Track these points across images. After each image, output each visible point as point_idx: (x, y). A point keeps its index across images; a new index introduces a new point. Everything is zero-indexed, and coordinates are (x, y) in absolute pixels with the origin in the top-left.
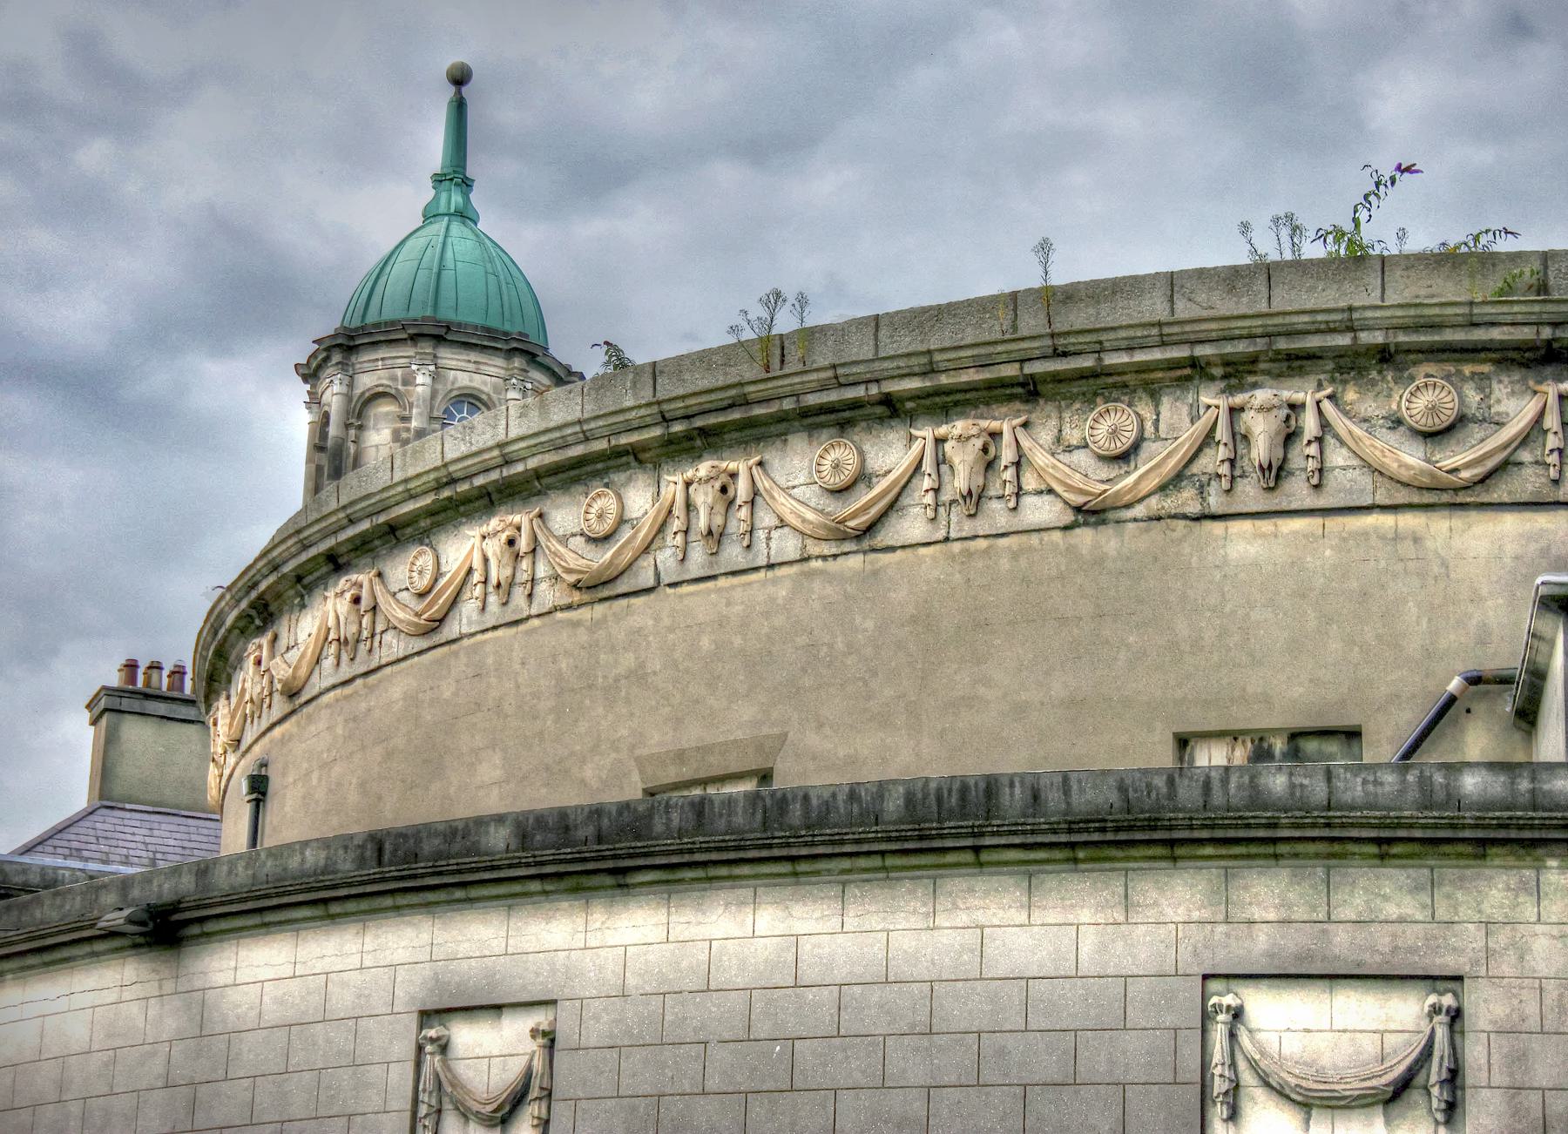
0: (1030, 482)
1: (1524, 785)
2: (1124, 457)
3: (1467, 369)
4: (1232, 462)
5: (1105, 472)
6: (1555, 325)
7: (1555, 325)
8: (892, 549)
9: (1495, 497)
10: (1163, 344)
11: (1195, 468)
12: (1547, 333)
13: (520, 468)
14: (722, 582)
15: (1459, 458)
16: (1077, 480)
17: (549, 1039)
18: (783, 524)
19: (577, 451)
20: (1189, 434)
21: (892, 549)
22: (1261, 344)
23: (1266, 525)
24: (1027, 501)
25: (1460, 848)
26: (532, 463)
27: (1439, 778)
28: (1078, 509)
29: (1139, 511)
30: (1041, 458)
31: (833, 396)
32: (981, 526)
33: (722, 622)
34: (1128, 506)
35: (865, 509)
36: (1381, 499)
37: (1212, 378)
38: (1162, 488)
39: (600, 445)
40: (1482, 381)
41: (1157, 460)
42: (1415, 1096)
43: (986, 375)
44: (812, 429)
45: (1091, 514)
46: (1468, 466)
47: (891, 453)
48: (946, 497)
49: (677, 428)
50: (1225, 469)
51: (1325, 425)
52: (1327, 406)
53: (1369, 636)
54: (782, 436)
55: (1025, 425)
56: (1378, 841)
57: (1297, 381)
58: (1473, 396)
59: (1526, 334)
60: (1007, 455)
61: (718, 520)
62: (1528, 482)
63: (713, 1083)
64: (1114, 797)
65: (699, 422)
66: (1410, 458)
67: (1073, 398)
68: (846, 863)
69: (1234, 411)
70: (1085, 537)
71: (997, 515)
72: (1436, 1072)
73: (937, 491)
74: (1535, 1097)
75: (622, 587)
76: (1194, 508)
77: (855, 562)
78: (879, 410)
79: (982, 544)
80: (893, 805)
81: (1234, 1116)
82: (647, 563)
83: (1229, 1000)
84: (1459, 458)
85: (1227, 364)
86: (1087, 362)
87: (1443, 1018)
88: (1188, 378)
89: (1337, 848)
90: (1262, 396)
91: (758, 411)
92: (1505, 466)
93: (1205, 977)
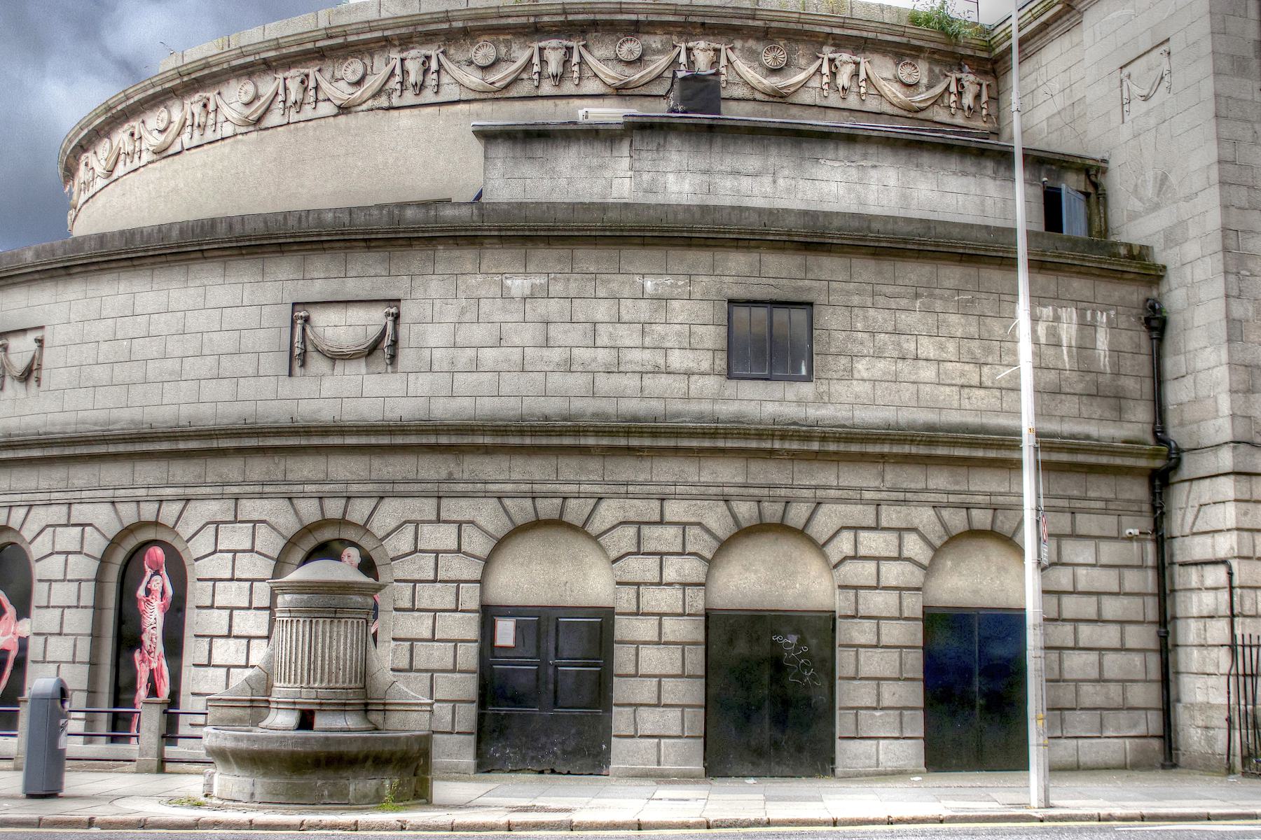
0: (321, 97)
1: (432, 213)
2: (359, 83)
3: (501, 38)
4: (402, 83)
5: (351, 90)
6: (536, 16)
7: (536, 16)
8: (267, 129)
9: (511, 95)
10: (371, 31)
11: (387, 87)
12: (532, 20)
13: (131, 101)
14: (206, 147)
15: (500, 76)
16: (339, 94)
17: (40, 342)
18: (227, 120)
19: (151, 92)
20: (385, 71)
21: (267, 129)
22: (411, 29)
23: (415, 111)
24: (320, 105)
25: (400, 242)
26: (136, 98)
27: (396, 212)
28: (339, 107)
29: (364, 107)
30: (324, 85)
31: (241, 61)
32: (302, 117)
33: (205, 165)
34: (359, 105)
35: (256, 111)
36: (463, 97)
37: (395, 46)
38: (374, 96)
39: (159, 89)
40: (508, 44)
41: (372, 83)
42: (378, 353)
43: (301, 48)
44: (238, 77)
45: (344, 109)
46: (499, 81)
47: (267, 85)
48: (288, 104)
49: (185, 79)
50: (398, 86)
51: (440, 65)
52: (442, 57)
53: (456, 159)
54: (227, 80)
55: (319, 71)
56: (365, 240)
57: (430, 46)
58: (503, 50)
59: (523, 20)
60: (312, 84)
61: (203, 120)
62: (525, 88)
63: (101, 359)
64: (262, 225)
65: (193, 76)
66: (473, 78)
67: (338, 58)
68: (152, 260)
69: (403, 60)
70: (342, 119)
71: (308, 111)
72: (387, 342)
73: (284, 102)
74: (427, 352)
75: (171, 151)
76: (386, 104)
77: (254, 135)
78: (263, 67)
79: (302, 124)
80: (175, 233)
81: (303, 365)
82: (178, 140)
83: (302, 314)
84: (500, 76)
85: (400, 39)
86: (340, 40)
87: (390, 318)
88: (385, 46)
89: (348, 244)
90: (413, 53)
91: (214, 69)
92: (516, 80)
93: (294, 304)
